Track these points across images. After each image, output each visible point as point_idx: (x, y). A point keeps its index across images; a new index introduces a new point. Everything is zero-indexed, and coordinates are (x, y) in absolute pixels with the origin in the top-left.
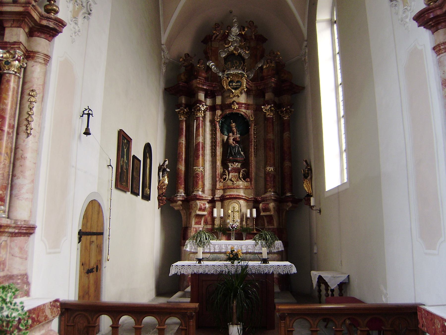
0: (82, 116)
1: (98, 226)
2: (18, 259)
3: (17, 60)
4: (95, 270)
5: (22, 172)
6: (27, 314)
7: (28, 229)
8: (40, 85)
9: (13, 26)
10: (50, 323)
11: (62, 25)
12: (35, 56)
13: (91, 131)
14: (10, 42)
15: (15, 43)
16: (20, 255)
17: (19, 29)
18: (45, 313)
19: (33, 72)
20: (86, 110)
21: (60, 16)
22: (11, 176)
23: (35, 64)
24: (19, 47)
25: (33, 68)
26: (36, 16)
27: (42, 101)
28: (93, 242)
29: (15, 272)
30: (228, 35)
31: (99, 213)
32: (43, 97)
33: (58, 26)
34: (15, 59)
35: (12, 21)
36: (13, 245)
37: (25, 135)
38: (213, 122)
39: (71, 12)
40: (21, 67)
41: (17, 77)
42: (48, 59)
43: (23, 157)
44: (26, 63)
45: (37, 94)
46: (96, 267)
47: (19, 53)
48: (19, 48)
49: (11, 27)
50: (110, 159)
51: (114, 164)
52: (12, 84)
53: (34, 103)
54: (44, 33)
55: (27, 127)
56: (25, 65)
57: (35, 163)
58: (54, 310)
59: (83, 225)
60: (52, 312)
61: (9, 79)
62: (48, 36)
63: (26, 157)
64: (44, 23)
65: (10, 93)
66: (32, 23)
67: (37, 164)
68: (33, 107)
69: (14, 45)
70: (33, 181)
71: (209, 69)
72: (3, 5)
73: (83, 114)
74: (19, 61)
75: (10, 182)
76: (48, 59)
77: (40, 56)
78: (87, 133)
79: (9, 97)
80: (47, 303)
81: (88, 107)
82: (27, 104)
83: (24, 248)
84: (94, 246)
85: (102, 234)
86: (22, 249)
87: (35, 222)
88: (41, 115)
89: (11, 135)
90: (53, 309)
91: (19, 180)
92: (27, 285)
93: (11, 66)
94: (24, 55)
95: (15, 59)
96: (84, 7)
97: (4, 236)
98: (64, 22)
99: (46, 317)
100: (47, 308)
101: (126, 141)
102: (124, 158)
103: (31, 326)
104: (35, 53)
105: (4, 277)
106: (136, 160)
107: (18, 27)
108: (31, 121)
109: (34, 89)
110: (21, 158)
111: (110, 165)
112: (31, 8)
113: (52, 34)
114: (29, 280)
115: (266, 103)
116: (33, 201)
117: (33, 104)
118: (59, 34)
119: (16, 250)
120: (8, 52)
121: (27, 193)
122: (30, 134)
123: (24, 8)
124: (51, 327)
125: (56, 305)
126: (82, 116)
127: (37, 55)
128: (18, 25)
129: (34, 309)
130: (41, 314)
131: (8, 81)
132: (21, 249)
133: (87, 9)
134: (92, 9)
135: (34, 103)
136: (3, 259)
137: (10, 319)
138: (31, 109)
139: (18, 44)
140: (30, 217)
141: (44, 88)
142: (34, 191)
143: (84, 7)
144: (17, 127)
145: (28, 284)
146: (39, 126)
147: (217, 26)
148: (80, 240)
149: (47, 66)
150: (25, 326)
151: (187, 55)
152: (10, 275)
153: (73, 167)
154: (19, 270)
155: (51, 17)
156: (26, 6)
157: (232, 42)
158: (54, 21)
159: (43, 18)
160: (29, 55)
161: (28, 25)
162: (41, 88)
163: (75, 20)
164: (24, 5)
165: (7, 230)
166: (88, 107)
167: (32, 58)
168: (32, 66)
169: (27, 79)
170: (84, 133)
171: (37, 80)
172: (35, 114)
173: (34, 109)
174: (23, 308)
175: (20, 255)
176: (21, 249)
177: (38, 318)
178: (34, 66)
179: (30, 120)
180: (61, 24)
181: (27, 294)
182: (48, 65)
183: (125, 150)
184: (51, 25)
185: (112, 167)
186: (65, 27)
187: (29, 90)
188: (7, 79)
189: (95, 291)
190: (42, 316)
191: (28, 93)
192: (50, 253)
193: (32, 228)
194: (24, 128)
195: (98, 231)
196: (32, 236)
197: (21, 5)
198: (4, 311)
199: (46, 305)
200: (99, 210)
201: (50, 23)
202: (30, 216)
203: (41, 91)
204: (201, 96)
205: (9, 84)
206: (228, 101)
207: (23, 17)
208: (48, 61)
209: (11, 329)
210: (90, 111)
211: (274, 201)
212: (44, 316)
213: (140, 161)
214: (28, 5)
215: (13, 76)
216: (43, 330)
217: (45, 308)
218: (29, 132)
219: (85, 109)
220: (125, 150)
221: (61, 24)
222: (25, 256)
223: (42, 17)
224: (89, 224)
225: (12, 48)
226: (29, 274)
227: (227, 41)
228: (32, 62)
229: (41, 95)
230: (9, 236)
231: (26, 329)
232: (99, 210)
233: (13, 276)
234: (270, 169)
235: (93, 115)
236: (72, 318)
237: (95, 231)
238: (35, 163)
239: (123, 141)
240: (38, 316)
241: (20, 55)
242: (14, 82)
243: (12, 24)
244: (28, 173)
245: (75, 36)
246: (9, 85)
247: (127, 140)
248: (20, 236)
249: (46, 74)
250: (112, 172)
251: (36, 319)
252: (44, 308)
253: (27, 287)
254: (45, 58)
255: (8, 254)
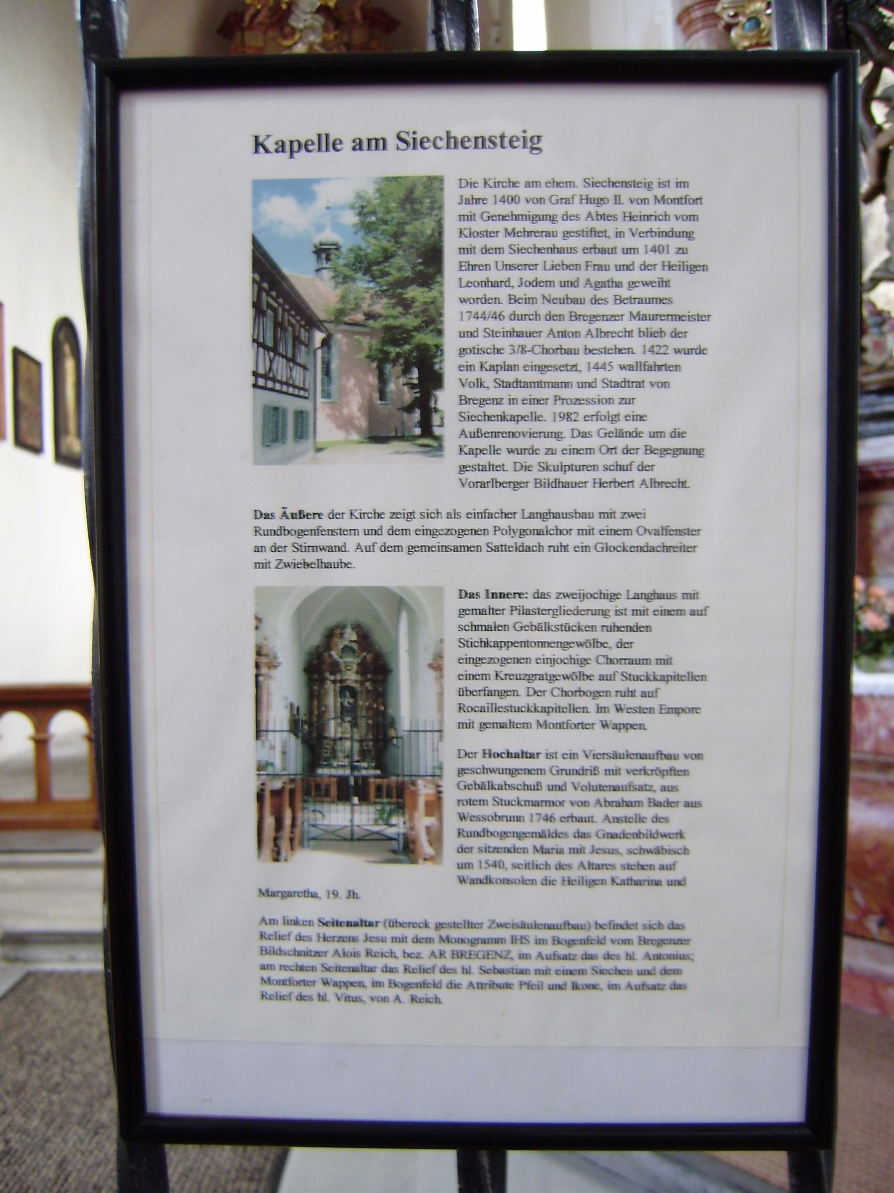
30: (289, 12)
38: (334, 690)
71: (330, 656)
106: (23, 362)
115: (367, 680)
147: (337, 627)
151: (318, 647)
157: (301, 31)
180: (280, 663)
204: (327, 675)
206: (345, 678)
211: (373, 740)
213: (38, 364)
221: (280, 663)
227: (287, 30)
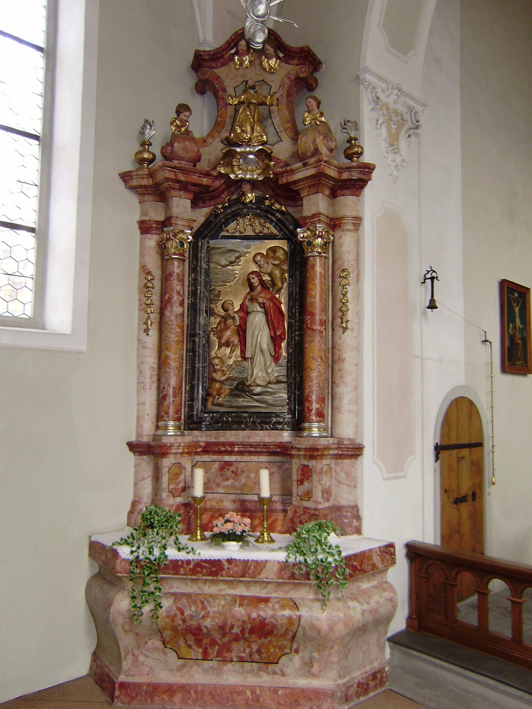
0: (424, 282)
1: (470, 434)
2: (345, 486)
3: (319, 237)
4: (470, 498)
5: (341, 377)
6: (344, 561)
7: (352, 451)
8: (352, 260)
9: (310, 193)
10: (384, 573)
11: (369, 169)
12: (341, 224)
13: (437, 304)
14: (309, 216)
15: (314, 216)
16: (347, 482)
17: (317, 195)
18: (372, 560)
19: (341, 246)
20: (428, 272)
21: (366, 158)
22: (330, 383)
23: (343, 233)
24: (320, 220)
25: (341, 241)
26: (332, 172)
27: (358, 281)
28: (463, 458)
29: (343, 502)
31: (470, 415)
32: (358, 275)
33: (363, 174)
34: (316, 236)
35: (308, 187)
36: (338, 469)
37: (341, 331)
39: (385, 140)
40: (326, 244)
41: (323, 258)
42: (358, 222)
43: (341, 359)
44: (333, 236)
45: (349, 274)
46: (471, 493)
47: (320, 227)
48: (320, 221)
49: (308, 195)
50: (485, 332)
51: (495, 337)
52: (318, 269)
53: (347, 286)
54: (348, 188)
55: (342, 318)
56: (332, 238)
57: (356, 365)
58: (386, 558)
59: (442, 435)
60: (382, 561)
61: (314, 263)
62: (355, 190)
63: (345, 359)
64: (345, 176)
65: (317, 281)
66: (330, 182)
67: (359, 365)
68: (346, 293)
69: (313, 218)
70: (356, 388)
72: (294, 172)
73: (425, 279)
74: (321, 237)
75: (330, 391)
76: (358, 222)
77: (347, 221)
78: (432, 306)
79: (316, 287)
80: (374, 549)
81: (431, 267)
82: (339, 289)
83: (350, 473)
84: (465, 465)
85: (480, 445)
86: (348, 475)
87: (363, 440)
88: (358, 299)
89: (324, 334)
90: (384, 556)
91: (339, 388)
92: (356, 519)
93: (314, 246)
94: (329, 225)
95: (316, 236)
96: (407, 121)
97: (326, 459)
98: (370, 165)
99: (374, 566)
100: (374, 554)
101: (516, 295)
102: (514, 322)
103: (351, 576)
104: (341, 219)
105: (330, 507)
107: (316, 193)
108: (345, 311)
109: (345, 268)
110: (338, 360)
111: (486, 341)
112: (324, 165)
113: (359, 187)
114: (360, 513)
116: (358, 413)
117: (346, 288)
118: (368, 182)
119: (342, 476)
120: (308, 229)
121: (350, 404)
122: (346, 328)
123: (316, 169)
124: (386, 579)
125: (389, 551)
126: (424, 282)
127: (343, 221)
128: (315, 191)
129: (355, 556)
130: (365, 561)
131: (314, 266)
132: (348, 474)
133: (412, 121)
134: (419, 118)
135: (347, 286)
136: (327, 487)
137: (325, 564)
138: (344, 295)
139: (318, 216)
140: (355, 434)
141: (358, 264)
142: (358, 401)
143: (407, 121)
144: (332, 321)
145: (358, 518)
146: (357, 315)
148: (437, 458)
149: (359, 232)
150: (343, 575)
152: (337, 506)
153: (417, 357)
154: (348, 500)
155: (353, 166)
156: (318, 166)
158: (356, 170)
159: (343, 171)
160: (335, 223)
161: (327, 185)
162: (355, 264)
163: (393, 149)
164: (315, 165)
165: (326, 453)
166: (431, 267)
167: (338, 226)
168: (340, 237)
169: (337, 256)
170: (428, 308)
171: (347, 255)
172: (349, 301)
173: (349, 295)
174: (340, 553)
175: (347, 482)
176: (348, 474)
177: (361, 566)
178: (341, 237)
179: (344, 311)
180: (369, 169)
181: (358, 531)
182: (360, 229)
183: (517, 310)
184: (354, 176)
185: (490, 342)
186: (374, 171)
187: (339, 271)
188: (311, 264)
189: (472, 529)
190: (368, 564)
191: (339, 274)
192: (388, 479)
193: (358, 448)
194: (339, 321)
195: (473, 441)
196: (360, 458)
197: (312, 166)
198: (318, 553)
199: (374, 551)
200: (471, 410)
201: (353, 174)
202: (357, 432)
203: (354, 269)
205: (314, 270)
207: (317, 180)
208: (359, 224)
209: (327, 576)
210: (434, 273)
212: (371, 565)
214: (319, 164)
215: (318, 259)
216: (373, 580)
217: (372, 554)
218: (345, 326)
219: (427, 271)
220: (517, 310)
221: (369, 169)
222: (353, 484)
223: (341, 169)
224: (453, 434)
225: (312, 223)
226: (360, 506)
228: (340, 232)
229: (355, 273)
230: (333, 458)
231: (345, 579)
232: (471, 410)
233: (341, 507)
234: (233, 37)
235: (438, 279)
236: (424, 568)
237: (465, 441)
238: (356, 365)
239: (510, 296)
240: (362, 564)
241: (321, 230)
242: (320, 265)
243: (309, 192)
244: (349, 379)
245: (397, 171)
246: (315, 272)
247: (518, 292)
248: (346, 459)
249: (358, 244)
250: (491, 351)
251: (359, 567)
252: (371, 554)
253: (356, 522)
254: (354, 222)
255: (334, 480)
